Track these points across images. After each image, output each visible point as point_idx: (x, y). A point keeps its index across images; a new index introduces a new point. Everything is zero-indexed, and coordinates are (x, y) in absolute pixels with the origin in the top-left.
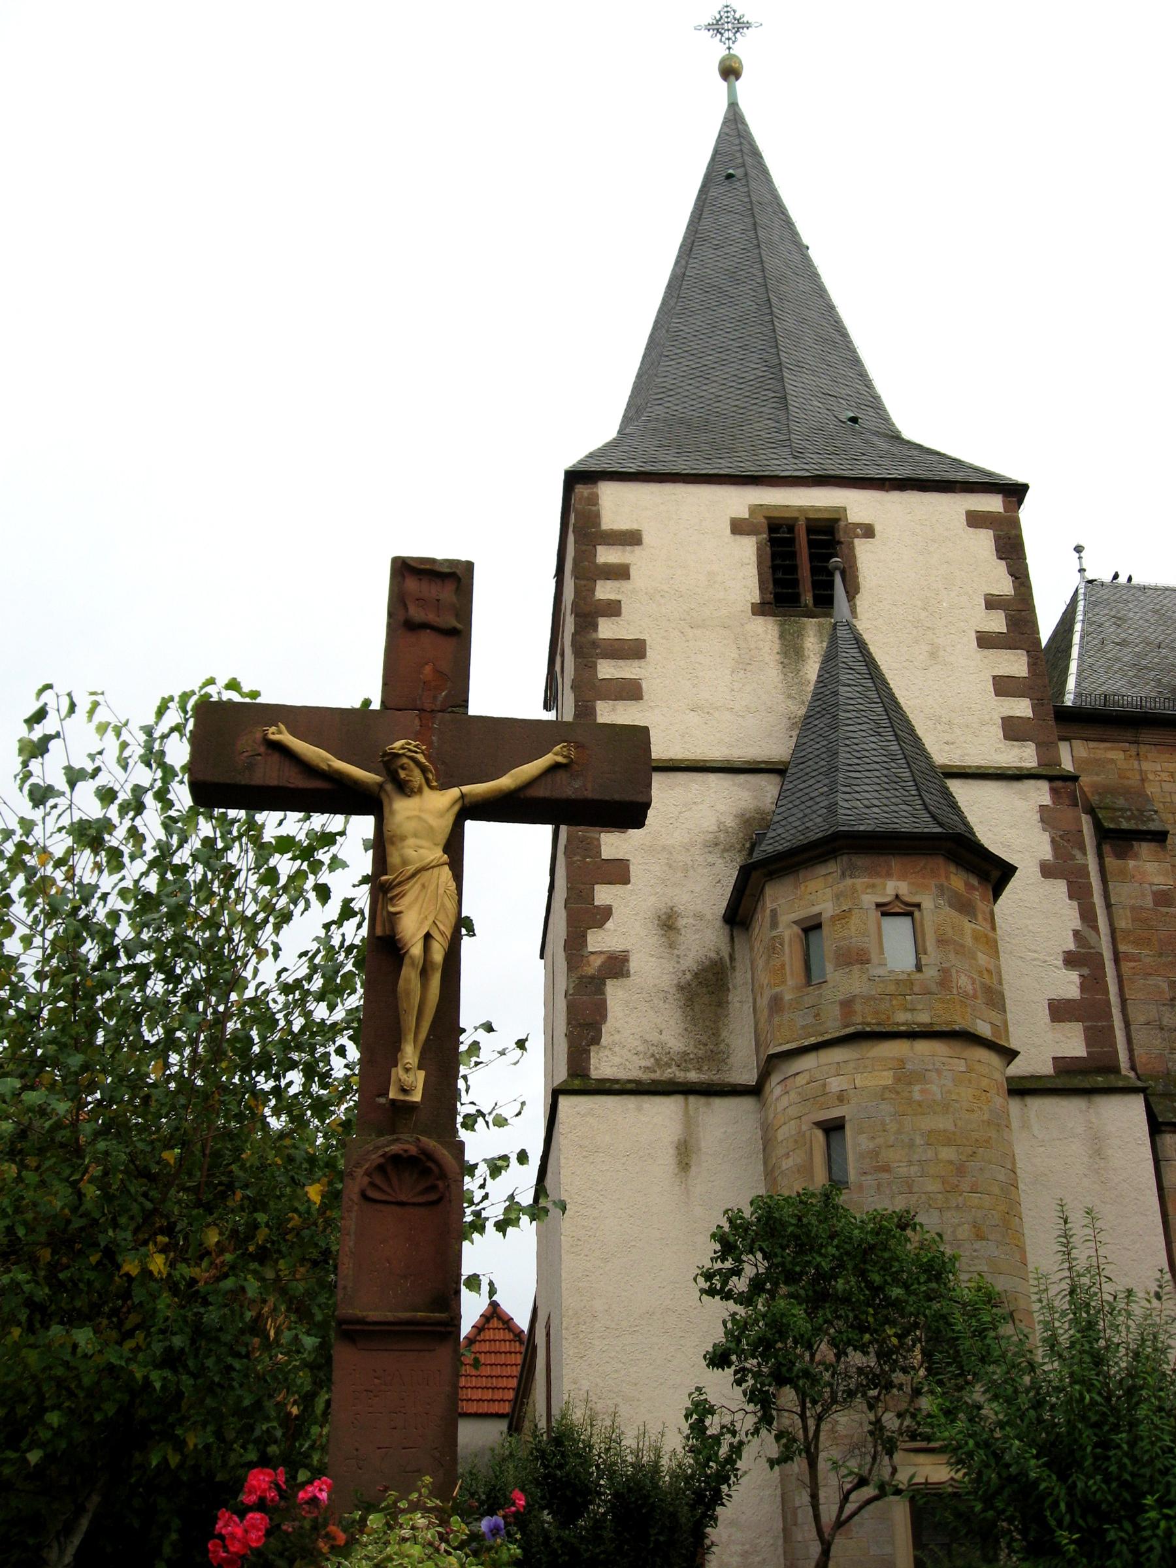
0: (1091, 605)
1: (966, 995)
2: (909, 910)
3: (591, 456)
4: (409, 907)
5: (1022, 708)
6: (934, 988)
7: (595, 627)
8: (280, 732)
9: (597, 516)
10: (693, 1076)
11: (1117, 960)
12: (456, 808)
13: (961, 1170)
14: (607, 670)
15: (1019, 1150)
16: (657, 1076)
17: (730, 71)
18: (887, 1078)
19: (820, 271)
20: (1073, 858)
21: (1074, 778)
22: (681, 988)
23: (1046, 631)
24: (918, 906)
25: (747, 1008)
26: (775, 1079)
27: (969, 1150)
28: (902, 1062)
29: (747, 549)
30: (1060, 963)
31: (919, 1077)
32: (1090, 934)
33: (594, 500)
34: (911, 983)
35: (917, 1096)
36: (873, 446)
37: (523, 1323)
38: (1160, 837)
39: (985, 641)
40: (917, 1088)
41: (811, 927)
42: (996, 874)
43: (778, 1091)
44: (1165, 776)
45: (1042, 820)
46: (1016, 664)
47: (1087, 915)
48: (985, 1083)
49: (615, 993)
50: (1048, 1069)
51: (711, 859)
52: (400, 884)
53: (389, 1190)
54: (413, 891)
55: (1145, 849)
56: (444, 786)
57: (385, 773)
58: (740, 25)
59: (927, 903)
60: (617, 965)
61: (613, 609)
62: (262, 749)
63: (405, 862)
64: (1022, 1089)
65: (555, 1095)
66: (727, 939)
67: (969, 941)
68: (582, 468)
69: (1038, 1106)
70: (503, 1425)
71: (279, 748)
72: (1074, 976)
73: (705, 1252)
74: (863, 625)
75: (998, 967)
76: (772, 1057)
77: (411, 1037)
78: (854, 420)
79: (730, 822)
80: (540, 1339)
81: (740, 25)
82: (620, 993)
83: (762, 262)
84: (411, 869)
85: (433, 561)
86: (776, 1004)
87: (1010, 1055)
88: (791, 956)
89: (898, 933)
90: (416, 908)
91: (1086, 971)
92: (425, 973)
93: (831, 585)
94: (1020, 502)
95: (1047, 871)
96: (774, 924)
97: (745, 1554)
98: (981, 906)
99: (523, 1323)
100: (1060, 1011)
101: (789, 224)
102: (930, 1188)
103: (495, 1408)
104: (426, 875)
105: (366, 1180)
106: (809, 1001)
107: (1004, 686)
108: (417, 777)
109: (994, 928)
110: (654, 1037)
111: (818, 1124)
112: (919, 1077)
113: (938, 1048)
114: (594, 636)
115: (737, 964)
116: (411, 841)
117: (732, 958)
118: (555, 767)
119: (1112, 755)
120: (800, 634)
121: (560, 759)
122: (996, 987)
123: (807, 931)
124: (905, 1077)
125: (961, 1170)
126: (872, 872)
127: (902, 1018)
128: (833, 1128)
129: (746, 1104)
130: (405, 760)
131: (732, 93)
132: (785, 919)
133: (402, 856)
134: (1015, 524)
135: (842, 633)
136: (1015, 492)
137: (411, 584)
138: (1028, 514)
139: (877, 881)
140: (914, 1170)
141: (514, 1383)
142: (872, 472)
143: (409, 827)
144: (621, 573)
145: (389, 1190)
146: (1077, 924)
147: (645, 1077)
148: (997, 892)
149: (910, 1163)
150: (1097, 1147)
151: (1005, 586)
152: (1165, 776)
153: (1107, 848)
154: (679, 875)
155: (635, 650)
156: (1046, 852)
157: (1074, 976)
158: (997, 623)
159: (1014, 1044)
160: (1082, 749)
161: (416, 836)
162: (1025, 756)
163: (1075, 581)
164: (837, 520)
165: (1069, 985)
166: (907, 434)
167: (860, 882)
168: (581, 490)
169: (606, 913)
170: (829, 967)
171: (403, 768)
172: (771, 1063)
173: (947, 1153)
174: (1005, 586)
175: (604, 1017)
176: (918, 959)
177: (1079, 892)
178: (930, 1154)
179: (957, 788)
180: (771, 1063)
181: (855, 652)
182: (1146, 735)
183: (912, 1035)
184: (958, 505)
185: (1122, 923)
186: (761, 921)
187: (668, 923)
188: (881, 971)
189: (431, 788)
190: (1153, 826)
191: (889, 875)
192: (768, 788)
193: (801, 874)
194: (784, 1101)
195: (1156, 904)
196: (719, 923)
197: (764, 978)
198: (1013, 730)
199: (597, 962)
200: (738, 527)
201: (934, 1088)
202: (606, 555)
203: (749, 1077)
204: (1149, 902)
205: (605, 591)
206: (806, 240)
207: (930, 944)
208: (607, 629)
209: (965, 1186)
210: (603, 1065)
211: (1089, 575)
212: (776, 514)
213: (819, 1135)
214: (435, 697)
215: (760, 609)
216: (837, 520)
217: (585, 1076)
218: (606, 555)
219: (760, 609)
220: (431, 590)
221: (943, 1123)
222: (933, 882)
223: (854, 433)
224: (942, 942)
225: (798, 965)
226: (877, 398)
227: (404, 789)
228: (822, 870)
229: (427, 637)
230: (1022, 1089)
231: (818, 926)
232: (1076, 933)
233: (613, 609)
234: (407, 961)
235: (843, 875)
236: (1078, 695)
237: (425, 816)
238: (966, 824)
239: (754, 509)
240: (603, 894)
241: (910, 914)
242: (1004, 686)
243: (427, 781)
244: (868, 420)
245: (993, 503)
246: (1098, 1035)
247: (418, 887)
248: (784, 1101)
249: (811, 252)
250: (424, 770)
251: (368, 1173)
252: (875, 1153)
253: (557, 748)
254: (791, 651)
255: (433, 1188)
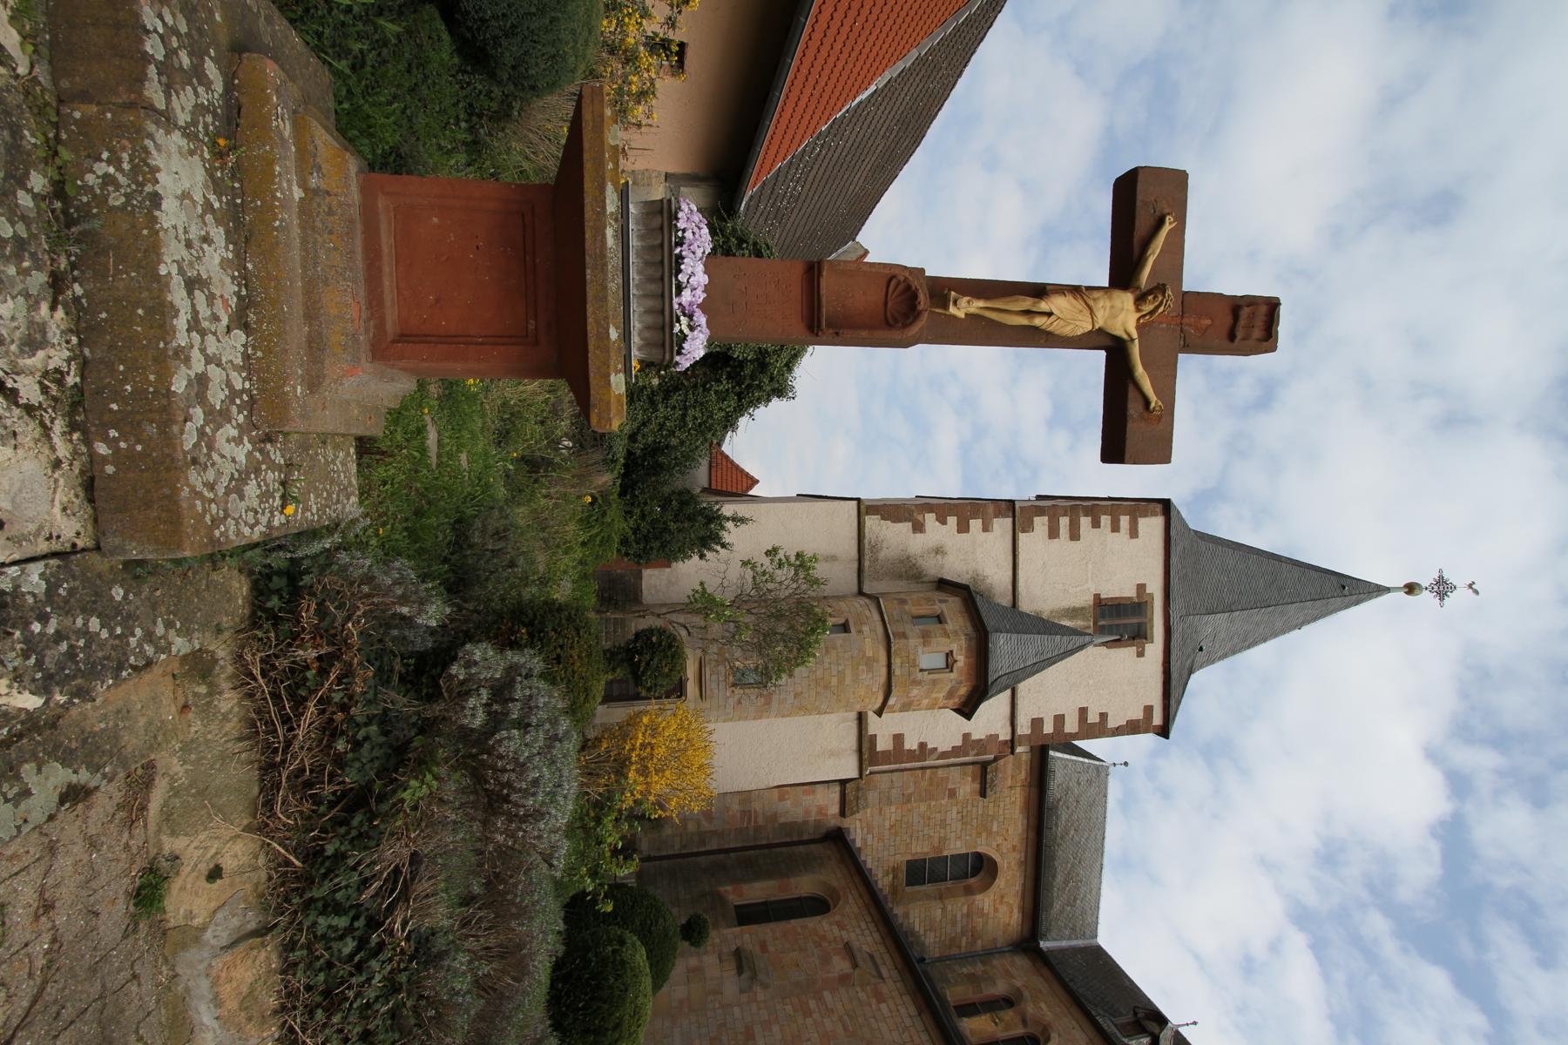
0: (1097, 768)
1: (908, 693)
2: (949, 665)
3: (1178, 512)
4: (1069, 301)
5: (1048, 728)
6: (912, 677)
7: (1086, 515)
8: (1170, 223)
9: (1146, 516)
10: (867, 563)
11: (922, 768)
12: (1125, 336)
13: (826, 687)
14: (1064, 522)
15: (833, 716)
16: (867, 546)
17: (1411, 589)
18: (869, 653)
19: (1287, 635)
20: (973, 749)
21: (1012, 753)
22: (908, 558)
23: (1081, 744)
24: (952, 671)
25: (899, 589)
26: (867, 601)
27: (836, 692)
28: (877, 661)
29: (1130, 592)
30: (922, 740)
31: (870, 669)
32: (935, 756)
33: (1154, 514)
34: (915, 666)
35: (861, 667)
36: (1187, 660)
37: (751, 493)
38: (983, 794)
39: (1083, 712)
40: (864, 667)
41: (940, 619)
42: (966, 710)
43: (861, 602)
44: (1013, 799)
45: (991, 735)
46: (1071, 726)
47: (944, 755)
48: (867, 700)
49: (906, 527)
50: (871, 732)
51: (971, 572)
52: (1082, 298)
53: (896, 294)
54: (1079, 305)
55: (977, 786)
56: (1138, 328)
57: (1148, 288)
58: (1442, 595)
59: (953, 676)
60: (919, 528)
61: (1096, 524)
62: (1158, 213)
63: (1094, 300)
64: (861, 718)
65: (858, 500)
66: (932, 579)
67: (934, 695)
68: (1172, 509)
69: (854, 725)
70: (706, 486)
71: (1160, 222)
72: (915, 747)
73: (789, 549)
74: (1090, 649)
75: (920, 709)
76: (877, 599)
77: (989, 304)
78: (1201, 649)
79: (988, 581)
80: (744, 498)
81: (1442, 595)
82: (906, 529)
83: (1292, 603)
84: (1091, 303)
85: (1278, 324)
86: (903, 602)
87: (879, 713)
88: (925, 609)
89: (939, 661)
90: (1069, 307)
91: (917, 753)
92: (1027, 313)
93: (1111, 633)
94: (1158, 734)
95: (966, 736)
96: (941, 601)
97: (655, 586)
98: (951, 703)
99: (751, 493)
100: (898, 739)
101: (1315, 619)
102: (818, 673)
103: (713, 483)
104: (1087, 312)
105: (902, 278)
106: (905, 617)
107: (1059, 720)
108: (1148, 308)
109: (940, 708)
110: (885, 545)
111: (847, 621)
112: (870, 669)
113: (883, 679)
114: (1081, 514)
115: (920, 585)
116: (1108, 304)
117: (923, 582)
118: (1147, 402)
119: (1023, 773)
120: (1085, 618)
121: (1153, 405)
122: (913, 707)
123: (938, 617)
124: (874, 659)
125: (826, 687)
126: (969, 649)
127: (896, 662)
128: (845, 628)
129: (855, 589)
130: (1160, 298)
131: (1397, 589)
132: (943, 606)
133: (1098, 298)
134: (1146, 731)
135: (1087, 639)
136: (1164, 731)
137: (1263, 309)
138: (1148, 740)
139: (964, 652)
140: (827, 665)
141: (724, 489)
142: (1173, 657)
143: (1118, 303)
144: (1115, 528)
145: (896, 294)
146: (940, 750)
147: (866, 541)
148: (957, 711)
149: (830, 664)
150: (833, 754)
151: (1112, 723)
152: (1013, 799)
153: (978, 766)
154: (963, 557)
155: (1075, 535)
156: (975, 737)
157: (915, 747)
158: (1093, 718)
159: (884, 715)
160: (1025, 758)
161: (1112, 307)
162: (1024, 728)
163: (1109, 760)
164: (1146, 638)
165: (911, 744)
166: (1193, 676)
167: (963, 642)
168: (1159, 507)
169: (944, 522)
170: (921, 627)
171: (1154, 298)
172: (874, 599)
173: (834, 681)
174: (1112, 723)
175: (894, 522)
176: (926, 670)
177: (956, 751)
178: (835, 673)
179: (1008, 692)
180: (874, 599)
181: (1077, 645)
182: (1034, 790)
183: (889, 666)
184: (1156, 700)
185: (940, 772)
186: (943, 596)
187: (939, 551)
188: (920, 651)
189: (1139, 319)
190: (988, 790)
191: (966, 657)
192: (1006, 601)
193: (966, 615)
194: (857, 605)
195: (950, 790)
196: (940, 576)
197: (915, 596)
198: (1037, 723)
199: (920, 518)
200: (1141, 588)
201: (865, 676)
202: (1124, 521)
203: (866, 589)
204: (950, 786)
205: (1105, 520)
206: (1305, 628)
207: (931, 676)
208: (1085, 522)
209: (819, 689)
210: (871, 522)
211: (1112, 768)
212: (1149, 607)
213: (842, 621)
214: (1190, 325)
215: (1097, 597)
216: (1146, 638)
217: (867, 513)
218: (1124, 521)
219: (1097, 597)
220: (1260, 322)
221: (848, 679)
222: (963, 679)
223: (1194, 650)
224: (934, 682)
225: (922, 612)
226: (1213, 662)
227: (1140, 300)
228: (968, 624)
229: (1228, 320)
230: (861, 718)
231: (940, 622)
232: (936, 749)
233: (1096, 524)
234: (1037, 300)
235: (966, 635)
236: (1053, 758)
237: (1124, 313)
238: (991, 697)
239: (1151, 595)
240: (952, 521)
241: (947, 667)
242: (1059, 720)
243: (1145, 316)
244: (1201, 656)
245: (1157, 720)
246: (886, 757)
247: (1081, 307)
248: (857, 605)
249: (1297, 631)
250: (1151, 313)
251: (906, 279)
252: (834, 648)
253: (1160, 403)
254: (1074, 612)
255: (896, 321)
